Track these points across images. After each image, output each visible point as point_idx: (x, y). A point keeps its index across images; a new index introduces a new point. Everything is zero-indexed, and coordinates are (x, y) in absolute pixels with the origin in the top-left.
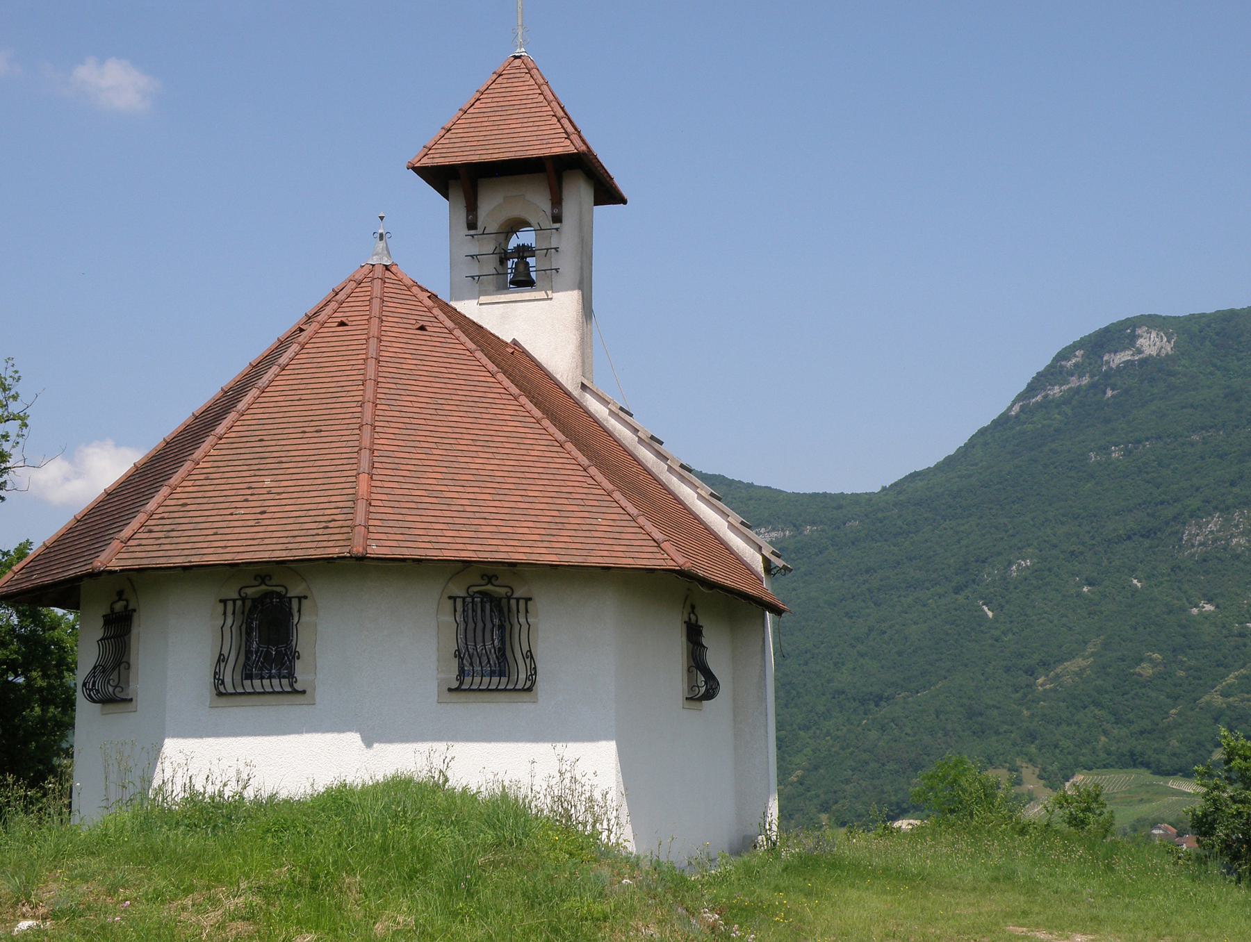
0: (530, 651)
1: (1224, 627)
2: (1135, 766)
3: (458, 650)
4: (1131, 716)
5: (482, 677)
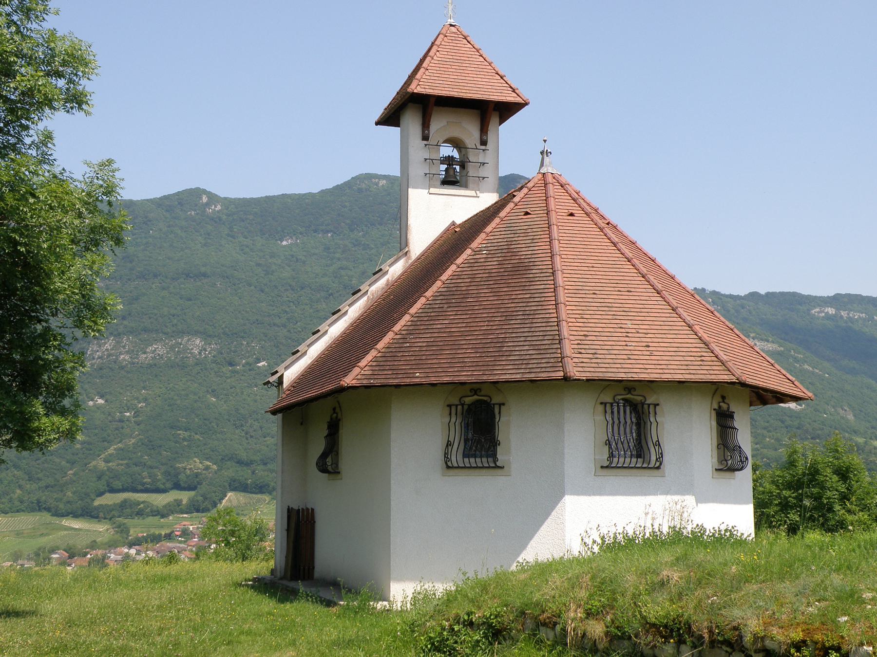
0: (658, 441)
1: (110, 415)
2: (40, 510)
3: (608, 440)
4: (40, 475)
5: (631, 458)
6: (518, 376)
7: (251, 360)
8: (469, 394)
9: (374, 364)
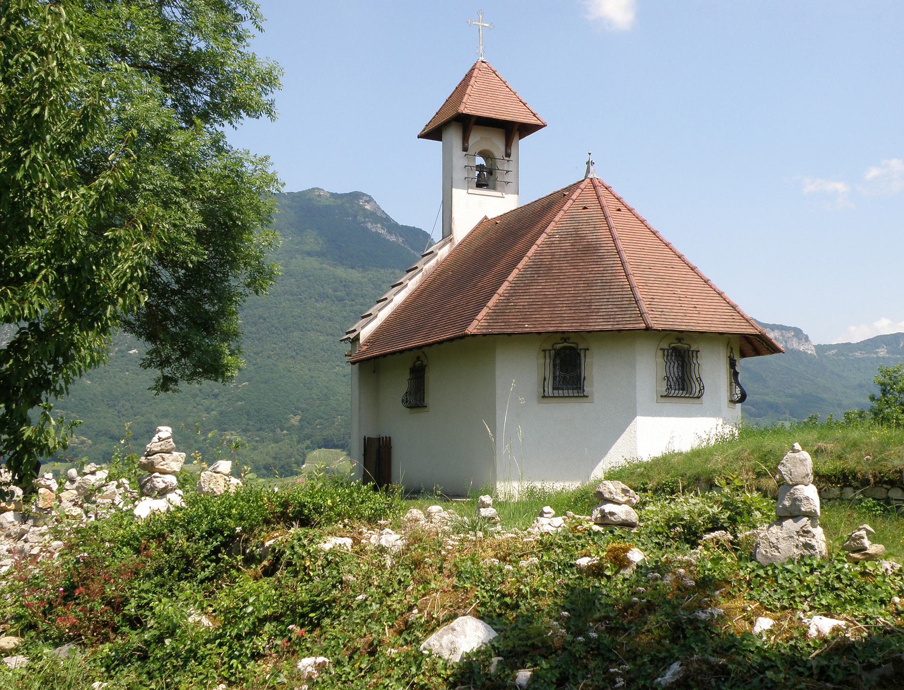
6: (609, 327)
7: (123, 348)
8: (560, 342)
9: (488, 318)
